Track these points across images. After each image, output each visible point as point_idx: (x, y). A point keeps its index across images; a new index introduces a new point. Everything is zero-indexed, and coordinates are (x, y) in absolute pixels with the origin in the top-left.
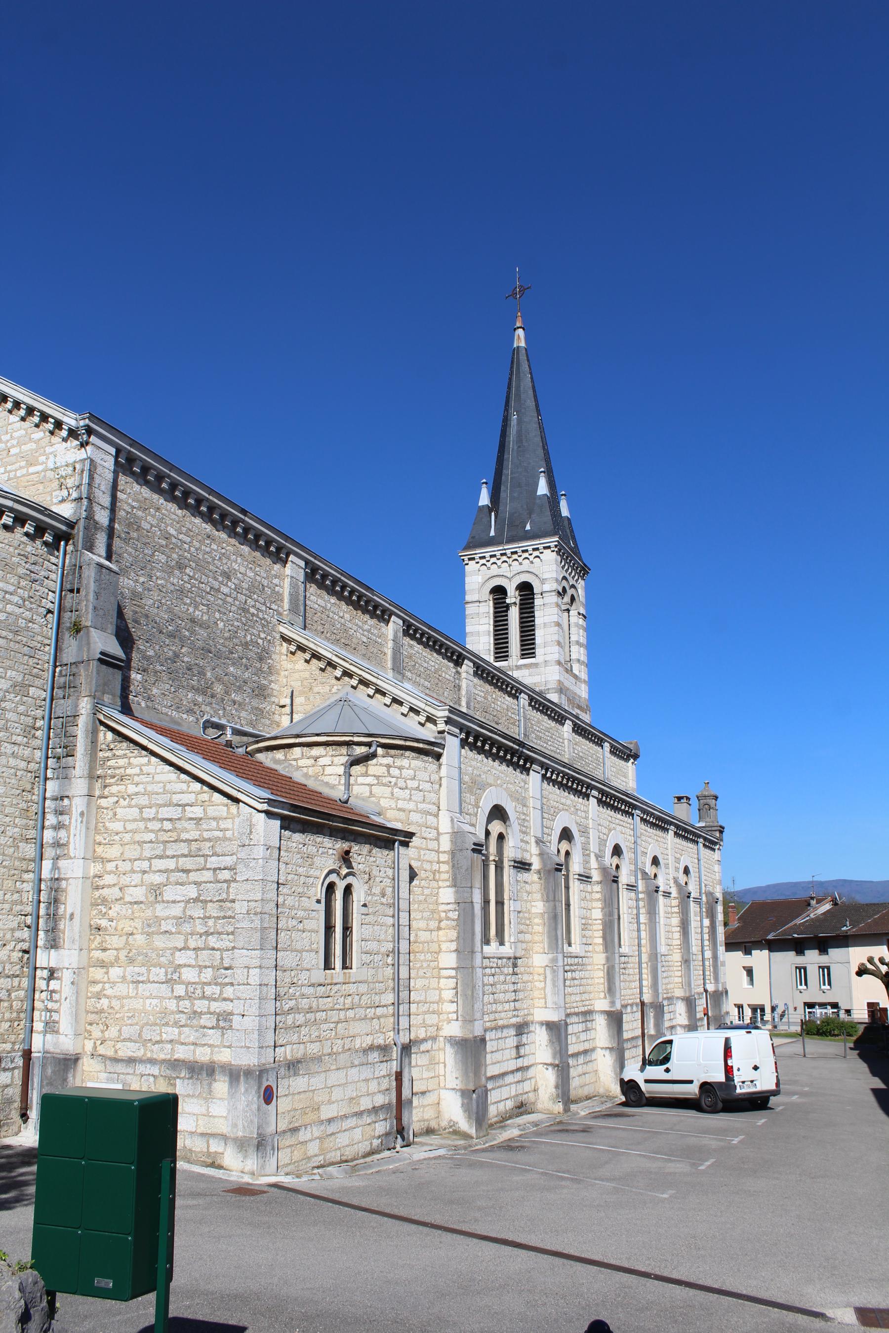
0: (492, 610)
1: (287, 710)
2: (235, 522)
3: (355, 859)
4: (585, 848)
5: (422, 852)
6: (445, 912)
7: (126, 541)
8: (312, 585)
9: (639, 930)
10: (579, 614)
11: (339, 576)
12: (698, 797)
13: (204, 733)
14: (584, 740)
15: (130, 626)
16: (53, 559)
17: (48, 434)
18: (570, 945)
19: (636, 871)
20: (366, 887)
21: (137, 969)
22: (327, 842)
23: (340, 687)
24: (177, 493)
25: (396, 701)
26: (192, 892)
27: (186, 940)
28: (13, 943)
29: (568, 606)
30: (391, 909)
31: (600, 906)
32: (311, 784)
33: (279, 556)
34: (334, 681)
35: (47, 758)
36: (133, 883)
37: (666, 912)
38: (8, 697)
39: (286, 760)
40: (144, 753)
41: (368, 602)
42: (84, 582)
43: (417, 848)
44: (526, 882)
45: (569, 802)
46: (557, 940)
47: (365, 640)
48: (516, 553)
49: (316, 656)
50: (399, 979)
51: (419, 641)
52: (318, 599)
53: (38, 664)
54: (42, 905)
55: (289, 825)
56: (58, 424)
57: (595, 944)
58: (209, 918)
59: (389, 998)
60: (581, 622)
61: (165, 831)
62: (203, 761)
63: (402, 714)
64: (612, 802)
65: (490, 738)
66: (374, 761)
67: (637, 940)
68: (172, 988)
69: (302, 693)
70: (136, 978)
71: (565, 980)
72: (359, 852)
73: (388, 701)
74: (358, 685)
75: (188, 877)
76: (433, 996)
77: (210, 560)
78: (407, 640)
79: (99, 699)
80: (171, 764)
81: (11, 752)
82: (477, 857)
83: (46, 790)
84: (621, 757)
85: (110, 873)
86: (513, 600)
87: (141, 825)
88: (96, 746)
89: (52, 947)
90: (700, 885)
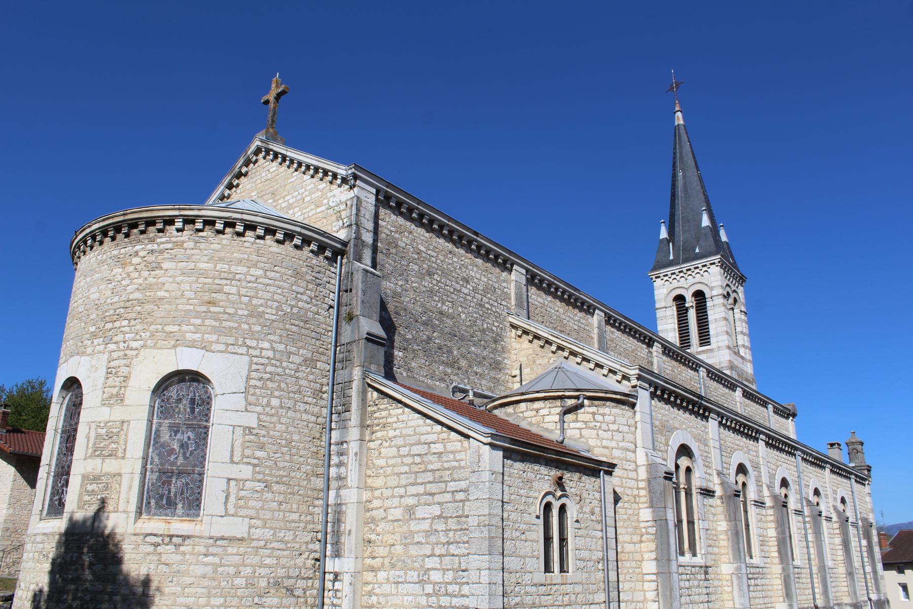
0: (675, 313)
1: (518, 379)
2: (470, 242)
3: (568, 484)
4: (758, 480)
5: (624, 481)
6: (645, 528)
7: (388, 255)
8: (533, 287)
9: (808, 547)
10: (741, 311)
11: (553, 280)
12: (847, 444)
13: (453, 396)
14: (752, 403)
15: (392, 316)
16: (333, 269)
17: (328, 184)
18: (751, 557)
19: (801, 499)
20: (578, 506)
21: (397, 573)
22: (544, 470)
23: (555, 359)
24: (424, 221)
25: (599, 366)
26: (436, 510)
27: (433, 549)
28: (307, 553)
29: (732, 306)
30: (600, 525)
31: (774, 526)
32: (534, 430)
33: (506, 266)
34: (551, 355)
35: (332, 414)
36: (394, 506)
37: (829, 534)
38: (301, 369)
39: (515, 413)
40: (400, 405)
41: (576, 300)
42: (355, 283)
43: (620, 477)
44: (711, 506)
45: (742, 444)
46: (740, 553)
47: (576, 327)
48: (689, 270)
49: (537, 337)
50: (608, 582)
51: (619, 329)
52: (537, 297)
53: (323, 345)
54: (329, 524)
55: (511, 455)
56: (335, 176)
57: (773, 557)
58: (450, 530)
59: (601, 597)
60: (743, 317)
61: (416, 464)
62: (457, 415)
63: (604, 375)
64: (777, 444)
65: (674, 392)
66: (582, 410)
67: (807, 555)
68: (423, 587)
69: (528, 365)
70: (397, 579)
71: (749, 586)
72: (571, 479)
73: (592, 366)
74: (569, 356)
75: (433, 499)
76: (639, 596)
77: (452, 269)
78: (609, 328)
79: (367, 368)
80: (419, 412)
81: (304, 409)
82: (669, 483)
83: (331, 438)
84: (780, 414)
85: (377, 498)
86: (691, 304)
87: (399, 460)
88: (366, 403)
89: (336, 556)
90: (856, 512)
